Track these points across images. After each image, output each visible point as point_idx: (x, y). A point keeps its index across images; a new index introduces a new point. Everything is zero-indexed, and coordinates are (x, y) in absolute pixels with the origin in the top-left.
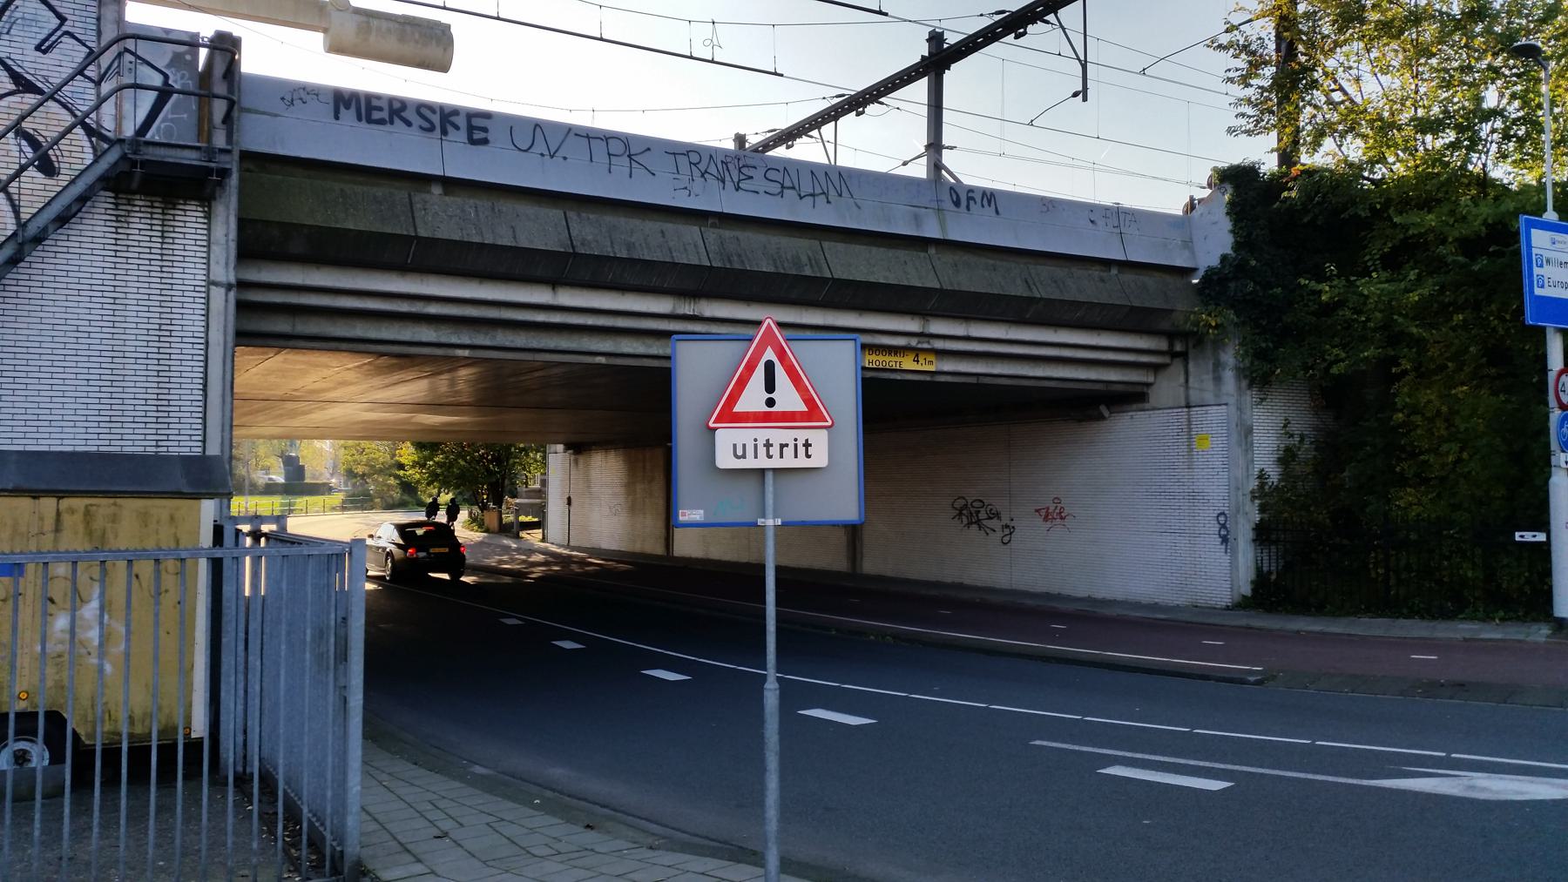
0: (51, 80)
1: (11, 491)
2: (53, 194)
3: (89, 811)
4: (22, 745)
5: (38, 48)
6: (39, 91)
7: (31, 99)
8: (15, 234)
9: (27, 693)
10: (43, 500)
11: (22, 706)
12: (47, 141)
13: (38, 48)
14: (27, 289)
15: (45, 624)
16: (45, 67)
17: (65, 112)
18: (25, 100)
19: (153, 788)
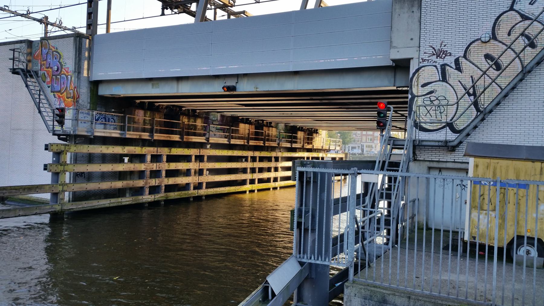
0: (534, 14)
1: (525, 159)
2: (536, 55)
3: (405, 255)
4: (528, 248)
5: (530, 4)
6: (530, 19)
7: (528, 22)
8: (522, 71)
9: (530, 230)
10: (536, 163)
11: (529, 234)
12: (533, 36)
13: (530, 4)
14: (525, 89)
15: (537, 208)
16: (532, 10)
17: (540, 24)
18: (525, 23)
19: (407, 249)
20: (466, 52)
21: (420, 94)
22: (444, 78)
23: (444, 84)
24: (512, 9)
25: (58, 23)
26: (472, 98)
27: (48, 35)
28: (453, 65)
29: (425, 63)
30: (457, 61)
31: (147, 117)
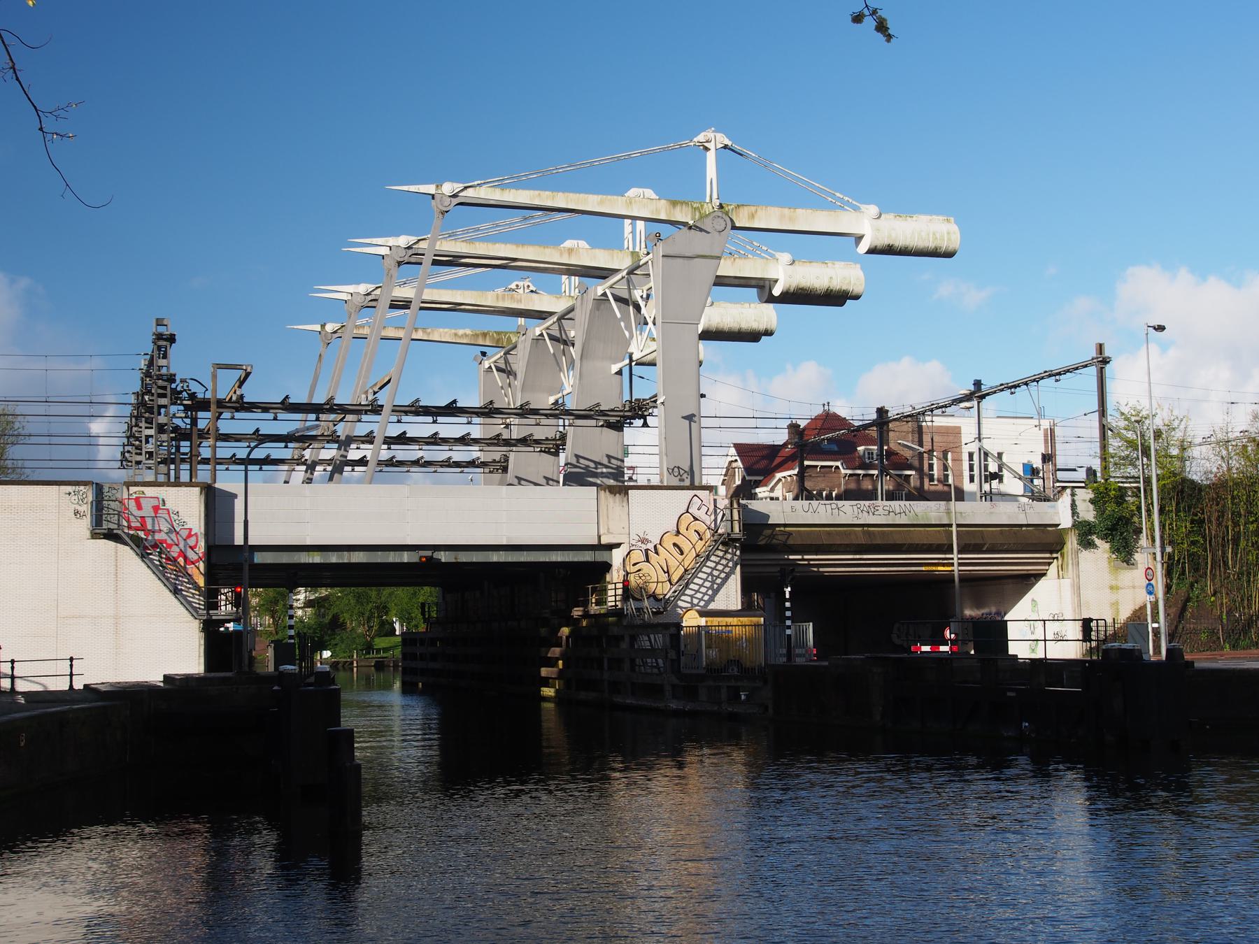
20: (661, 540)
21: (632, 572)
22: (648, 560)
23: (648, 564)
24: (687, 512)
25: (173, 422)
26: (667, 574)
27: (243, 467)
28: (653, 550)
29: (634, 548)
30: (655, 546)
31: (1204, 518)
